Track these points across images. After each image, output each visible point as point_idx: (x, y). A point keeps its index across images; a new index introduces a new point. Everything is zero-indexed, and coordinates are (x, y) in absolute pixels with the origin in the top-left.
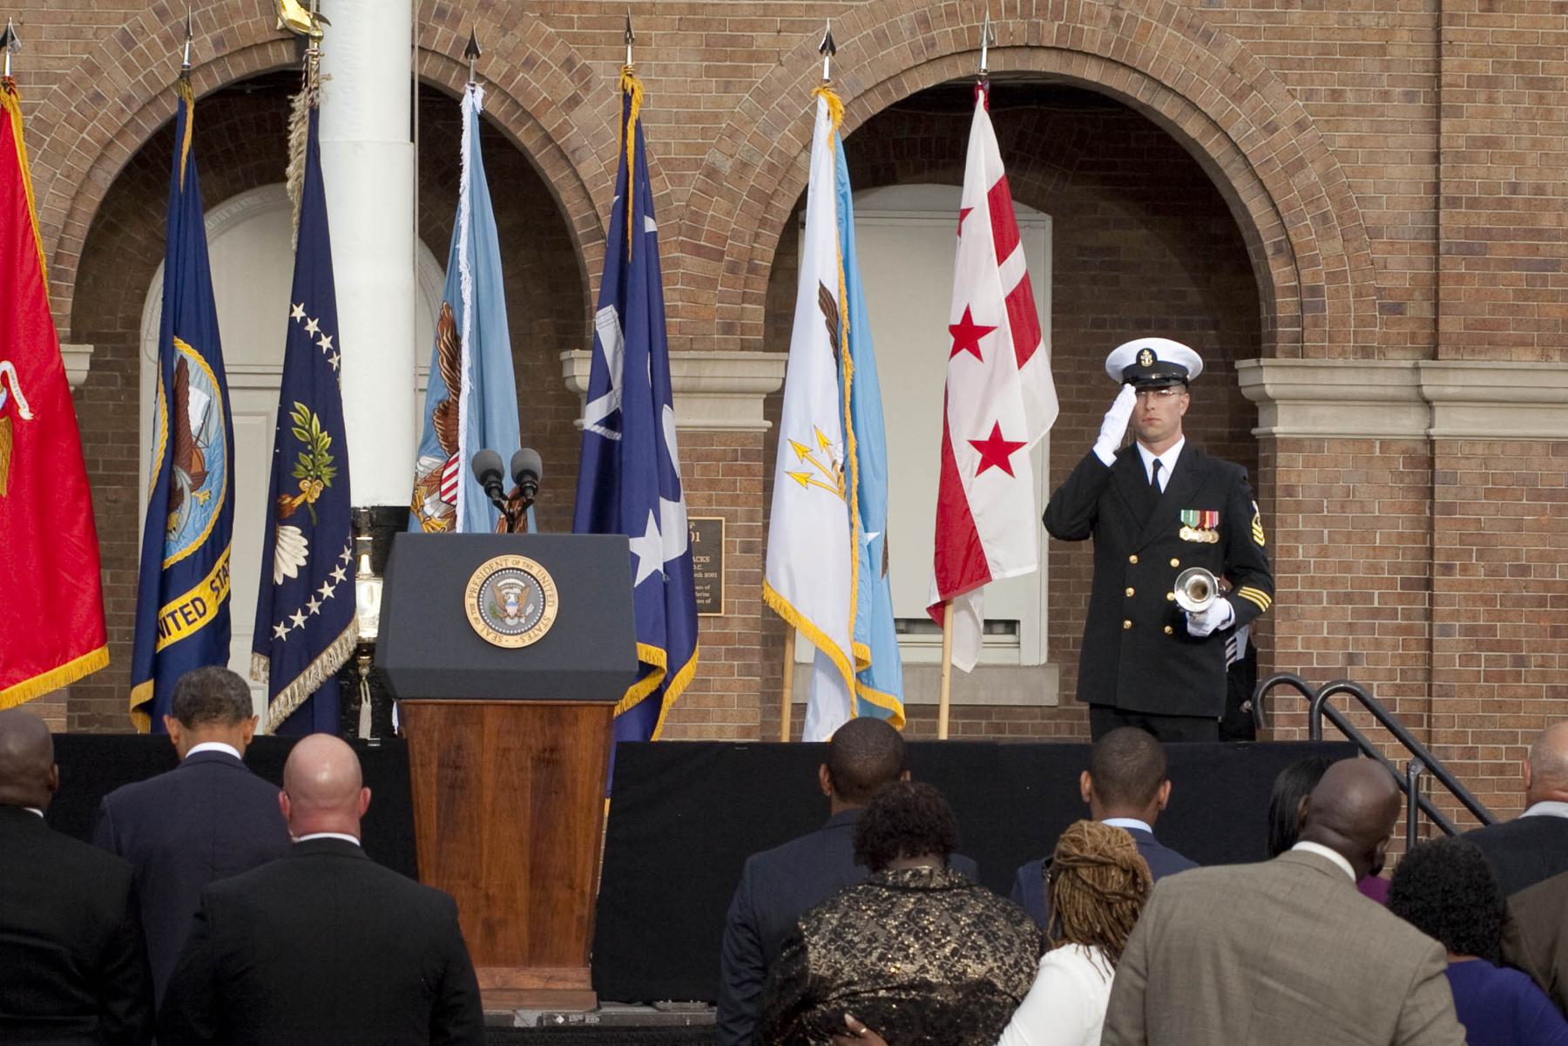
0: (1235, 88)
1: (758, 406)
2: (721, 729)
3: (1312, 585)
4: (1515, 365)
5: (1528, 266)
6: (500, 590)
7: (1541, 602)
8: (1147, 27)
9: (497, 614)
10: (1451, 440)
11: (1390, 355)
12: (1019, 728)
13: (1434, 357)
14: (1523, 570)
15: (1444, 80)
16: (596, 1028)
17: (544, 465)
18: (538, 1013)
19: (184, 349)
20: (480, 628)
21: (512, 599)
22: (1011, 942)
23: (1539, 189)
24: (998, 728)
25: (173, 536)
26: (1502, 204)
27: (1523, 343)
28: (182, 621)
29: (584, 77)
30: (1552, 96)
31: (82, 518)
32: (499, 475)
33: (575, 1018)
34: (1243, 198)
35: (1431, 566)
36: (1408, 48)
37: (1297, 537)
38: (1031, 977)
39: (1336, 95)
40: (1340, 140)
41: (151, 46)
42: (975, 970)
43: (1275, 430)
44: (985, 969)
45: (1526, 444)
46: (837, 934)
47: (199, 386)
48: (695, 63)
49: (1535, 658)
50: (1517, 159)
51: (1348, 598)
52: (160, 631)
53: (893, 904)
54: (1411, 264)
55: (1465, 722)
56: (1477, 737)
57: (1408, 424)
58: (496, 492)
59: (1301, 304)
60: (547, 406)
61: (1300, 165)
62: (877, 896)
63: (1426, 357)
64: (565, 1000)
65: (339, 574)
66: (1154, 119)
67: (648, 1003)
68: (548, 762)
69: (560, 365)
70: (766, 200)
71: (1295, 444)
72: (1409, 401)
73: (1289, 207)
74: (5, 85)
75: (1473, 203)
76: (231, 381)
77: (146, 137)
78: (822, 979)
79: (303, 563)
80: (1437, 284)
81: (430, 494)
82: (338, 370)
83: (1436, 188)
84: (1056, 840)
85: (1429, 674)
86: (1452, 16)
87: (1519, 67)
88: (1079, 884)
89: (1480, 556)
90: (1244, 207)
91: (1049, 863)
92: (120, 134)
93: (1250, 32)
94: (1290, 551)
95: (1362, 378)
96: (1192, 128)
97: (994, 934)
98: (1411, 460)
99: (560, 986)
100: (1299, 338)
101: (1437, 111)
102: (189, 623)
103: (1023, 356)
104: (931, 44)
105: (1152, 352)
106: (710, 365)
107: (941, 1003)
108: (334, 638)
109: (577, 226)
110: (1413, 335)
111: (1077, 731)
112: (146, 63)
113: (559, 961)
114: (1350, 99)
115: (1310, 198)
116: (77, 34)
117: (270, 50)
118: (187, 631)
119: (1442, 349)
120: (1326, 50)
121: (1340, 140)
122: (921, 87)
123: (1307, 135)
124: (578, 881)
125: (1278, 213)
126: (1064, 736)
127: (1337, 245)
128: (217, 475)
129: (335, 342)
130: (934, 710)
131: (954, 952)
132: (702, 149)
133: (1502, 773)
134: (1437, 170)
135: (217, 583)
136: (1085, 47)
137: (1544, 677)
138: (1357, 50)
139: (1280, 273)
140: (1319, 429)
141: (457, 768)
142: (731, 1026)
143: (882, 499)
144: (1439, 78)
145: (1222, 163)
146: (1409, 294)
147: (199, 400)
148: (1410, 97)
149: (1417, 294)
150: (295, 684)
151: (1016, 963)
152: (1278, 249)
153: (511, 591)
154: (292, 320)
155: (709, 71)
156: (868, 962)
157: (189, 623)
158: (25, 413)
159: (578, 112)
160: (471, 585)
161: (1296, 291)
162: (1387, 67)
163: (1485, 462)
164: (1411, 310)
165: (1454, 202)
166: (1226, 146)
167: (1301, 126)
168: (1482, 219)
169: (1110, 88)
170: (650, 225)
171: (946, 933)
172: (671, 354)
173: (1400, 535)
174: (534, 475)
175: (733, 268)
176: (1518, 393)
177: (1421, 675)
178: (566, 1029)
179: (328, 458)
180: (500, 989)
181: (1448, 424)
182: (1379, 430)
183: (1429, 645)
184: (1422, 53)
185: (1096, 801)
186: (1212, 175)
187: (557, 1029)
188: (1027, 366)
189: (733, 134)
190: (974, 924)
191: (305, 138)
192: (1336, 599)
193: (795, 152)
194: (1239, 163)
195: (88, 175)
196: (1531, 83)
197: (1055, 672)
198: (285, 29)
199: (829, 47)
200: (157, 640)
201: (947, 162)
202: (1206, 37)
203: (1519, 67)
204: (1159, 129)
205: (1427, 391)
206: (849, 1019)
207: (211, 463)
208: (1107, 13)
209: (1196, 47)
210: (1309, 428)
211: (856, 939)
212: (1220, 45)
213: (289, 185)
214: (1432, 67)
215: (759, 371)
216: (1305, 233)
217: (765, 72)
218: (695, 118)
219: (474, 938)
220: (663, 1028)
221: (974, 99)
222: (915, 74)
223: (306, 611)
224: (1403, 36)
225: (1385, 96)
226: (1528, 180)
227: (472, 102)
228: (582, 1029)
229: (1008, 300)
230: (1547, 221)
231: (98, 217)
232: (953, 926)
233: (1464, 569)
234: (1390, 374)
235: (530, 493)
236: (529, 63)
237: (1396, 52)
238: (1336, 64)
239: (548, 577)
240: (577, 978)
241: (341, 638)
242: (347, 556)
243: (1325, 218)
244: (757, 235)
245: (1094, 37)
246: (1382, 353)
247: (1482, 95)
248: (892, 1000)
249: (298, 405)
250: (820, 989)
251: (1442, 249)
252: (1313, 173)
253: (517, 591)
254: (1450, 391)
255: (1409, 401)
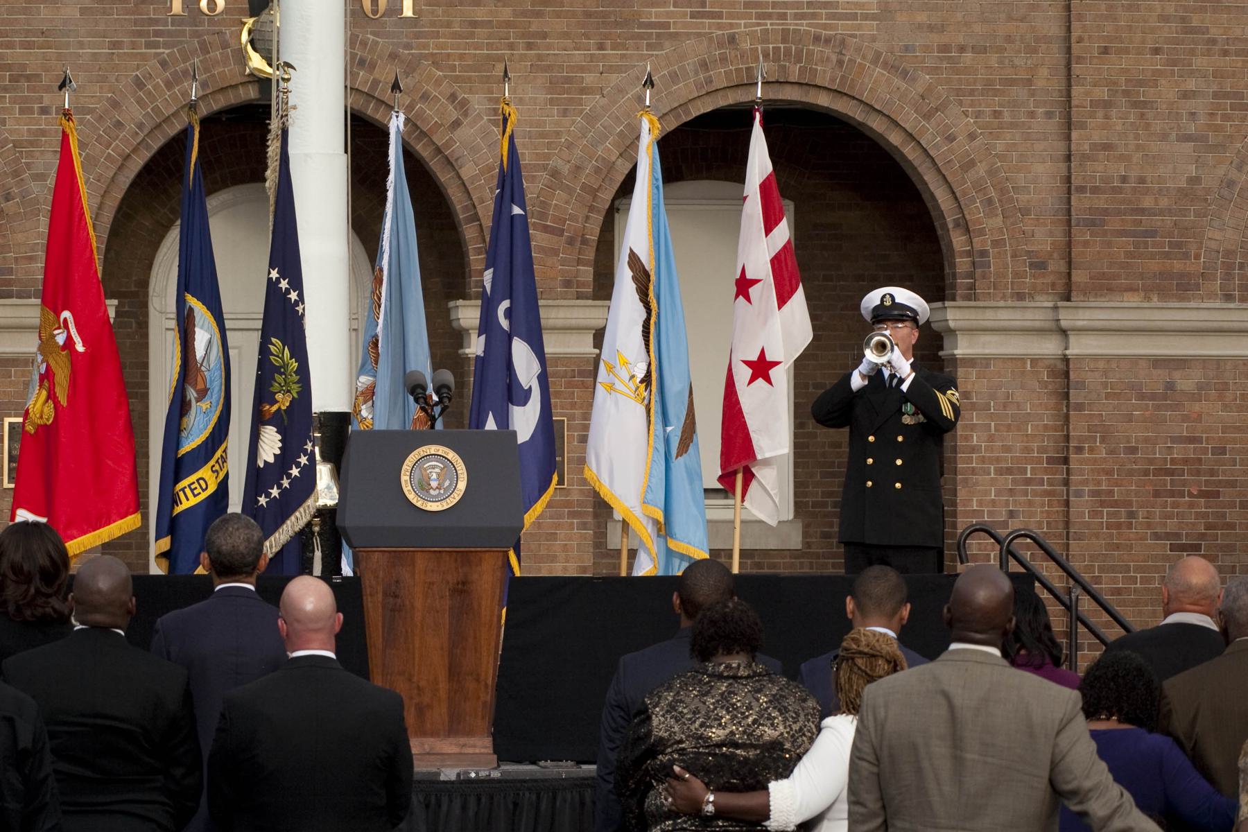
0: (926, 109)
1: (589, 339)
2: (565, 568)
3: (984, 462)
4: (1126, 305)
5: (1134, 234)
6: (426, 470)
7: (1146, 473)
8: (862, 66)
9: (423, 487)
10: (1081, 358)
11: (1037, 298)
12: (774, 566)
13: (1068, 300)
14: (1133, 450)
15: (1074, 103)
16: (498, 781)
17: (456, 382)
18: (456, 771)
19: (192, 301)
20: (411, 497)
21: (434, 476)
22: (798, 715)
23: (1142, 180)
24: (759, 565)
25: (184, 434)
26: (1118, 190)
27: (1131, 289)
28: (194, 492)
29: (463, 106)
30: (1150, 114)
31: (121, 423)
32: (424, 388)
33: (483, 774)
34: (932, 189)
35: (1068, 447)
36: (1047, 80)
37: (973, 428)
38: (812, 740)
39: (997, 114)
40: (1000, 145)
41: (156, 87)
42: (769, 733)
43: (956, 352)
44: (777, 733)
45: (1135, 360)
46: (672, 707)
47: (202, 328)
48: (542, 96)
49: (1141, 513)
50: (1122, 158)
51: (1009, 471)
52: (175, 501)
53: (712, 687)
54: (1051, 234)
55: (1093, 558)
56: (1101, 569)
57: (1049, 347)
58: (422, 400)
59: (974, 263)
60: (446, 340)
61: (972, 164)
62: (700, 681)
63: (1062, 300)
64: (475, 760)
65: (303, 460)
66: (868, 133)
67: (534, 763)
68: (462, 592)
69: (448, 310)
70: (594, 192)
71: (971, 362)
72: (1051, 331)
73: (965, 193)
74: (65, 115)
75: (1095, 190)
76: (228, 324)
77: (153, 152)
78: (661, 739)
79: (278, 452)
80: (1070, 247)
81: (365, 402)
82: (303, 315)
83: (1068, 179)
84: (842, 640)
85: (1067, 524)
86: (1079, 57)
87: (1126, 93)
88: (856, 669)
89: (1103, 440)
90: (932, 194)
91: (836, 657)
92: (135, 150)
93: (934, 70)
94: (967, 438)
95: (1018, 315)
96: (895, 138)
97: (785, 708)
98: (1053, 373)
99: (471, 751)
100: (972, 287)
101: (1069, 125)
102: (195, 496)
103: (782, 299)
104: (709, 81)
105: (891, 296)
106: (555, 310)
107: (745, 757)
108: (300, 505)
109: (459, 212)
110: (1053, 285)
111: (834, 566)
112: (153, 100)
113: (470, 733)
114: (1007, 118)
115: (979, 187)
116: (104, 79)
117: (241, 90)
118: (193, 501)
119: (1074, 294)
120: (989, 82)
121: (1000, 145)
122: (703, 111)
123: (977, 142)
124: (482, 677)
125: (956, 199)
126: (831, 571)
127: (998, 221)
128: (216, 389)
129: (301, 295)
130: (729, 553)
131: (755, 722)
132: (547, 157)
133: (1119, 594)
134: (1069, 168)
135: (217, 467)
136: (818, 82)
137: (1149, 525)
138: (1012, 82)
139: (958, 241)
140: (987, 351)
141: (396, 596)
142: (606, 777)
143: (676, 407)
144: (1069, 102)
145: (916, 163)
146: (1050, 254)
147: (203, 337)
148: (1049, 115)
149: (1055, 255)
150: (272, 538)
151: (801, 729)
152: (957, 225)
153: (434, 471)
154: (270, 280)
155: (552, 102)
156: (692, 728)
157: (195, 496)
158: (80, 348)
159: (459, 131)
160: (405, 467)
161: (969, 254)
162: (1032, 94)
163: (1105, 373)
164: (1052, 266)
165: (1081, 189)
166: (919, 152)
167: (972, 137)
168: (1101, 202)
169: (836, 111)
170: (517, 210)
171: (749, 708)
172: (541, 302)
173: (1046, 427)
174: (449, 388)
175: (571, 241)
176: (1116, 325)
177: (1061, 525)
178: (477, 781)
179: (295, 378)
180: (428, 754)
181: (1079, 347)
182: (1030, 351)
183: (1067, 503)
184: (1057, 84)
185: (857, 614)
186: (909, 172)
187: (471, 781)
188: (786, 307)
189: (570, 146)
190: (770, 701)
191: (279, 151)
192: (1000, 472)
193: (613, 159)
194: (928, 164)
195: (113, 179)
196: (1136, 105)
197: (799, 526)
198: (251, 75)
199: (650, 83)
200: (173, 508)
201: (732, 166)
202: (904, 74)
203: (1126, 93)
204: (871, 139)
205: (1063, 324)
206: (677, 769)
207: (211, 382)
208: (834, 58)
209: (897, 81)
210: (980, 351)
211: (685, 711)
212: (914, 80)
213: (267, 184)
214: (1064, 93)
215: (588, 313)
216: (976, 212)
217: (592, 102)
218: (543, 135)
219: (410, 718)
220: (546, 780)
221: (754, 118)
222: (699, 102)
223: (280, 486)
224: (1044, 72)
225: (1032, 115)
226: (1133, 174)
227: (396, 124)
228: (489, 781)
229: (772, 261)
230: (1147, 202)
231: (120, 209)
232: (754, 704)
233: (1091, 450)
234: (1037, 312)
235: (446, 400)
236: (425, 97)
237: (1040, 83)
238: (996, 93)
239: (460, 460)
240: (482, 745)
241: (305, 505)
242: (309, 447)
243: (990, 201)
244: (587, 217)
245: (825, 75)
246: (1032, 297)
247: (1100, 113)
248: (709, 754)
249: (274, 340)
250: (659, 746)
251: (1073, 223)
252: (981, 169)
253: (437, 470)
254: (1080, 323)
255: (1051, 331)
